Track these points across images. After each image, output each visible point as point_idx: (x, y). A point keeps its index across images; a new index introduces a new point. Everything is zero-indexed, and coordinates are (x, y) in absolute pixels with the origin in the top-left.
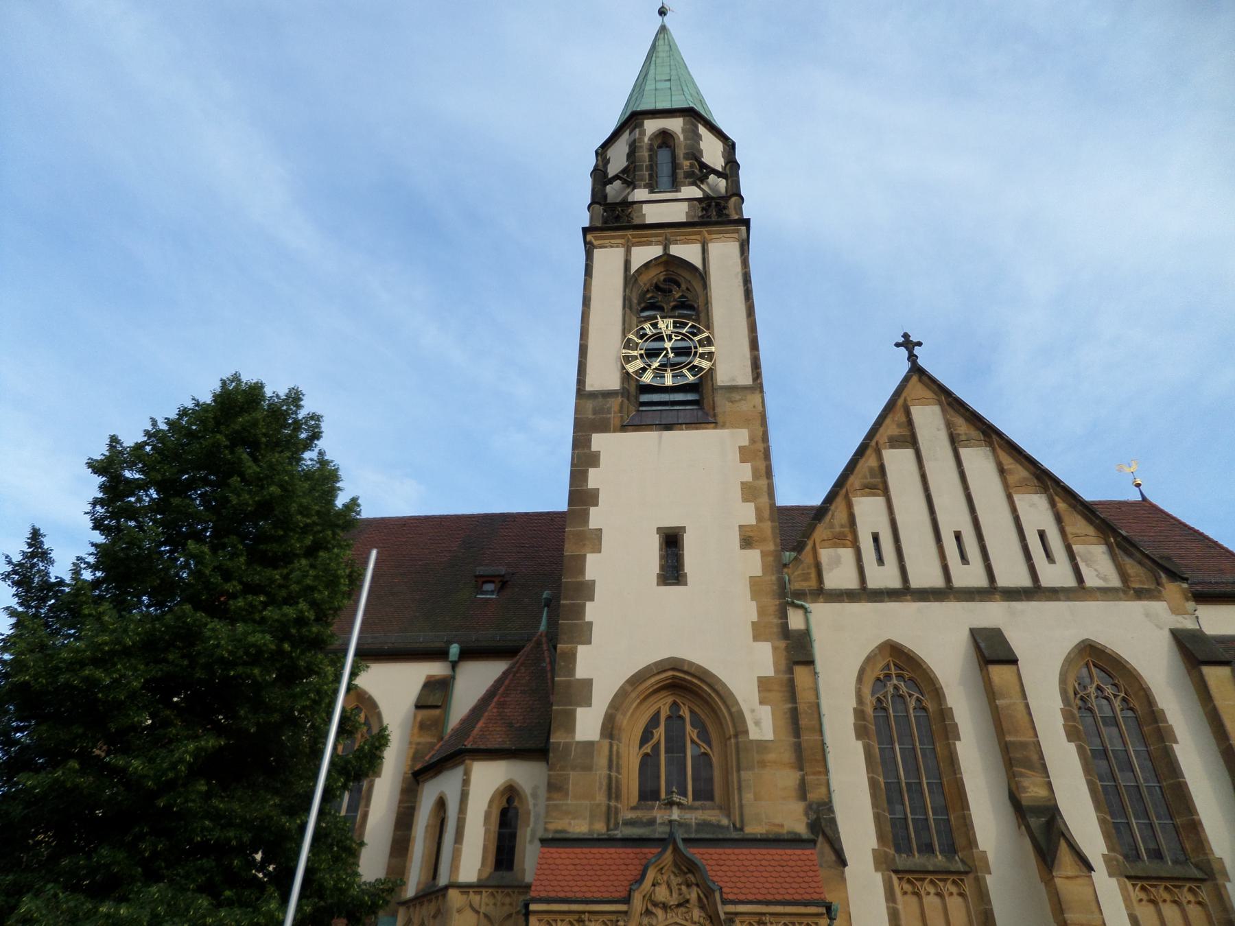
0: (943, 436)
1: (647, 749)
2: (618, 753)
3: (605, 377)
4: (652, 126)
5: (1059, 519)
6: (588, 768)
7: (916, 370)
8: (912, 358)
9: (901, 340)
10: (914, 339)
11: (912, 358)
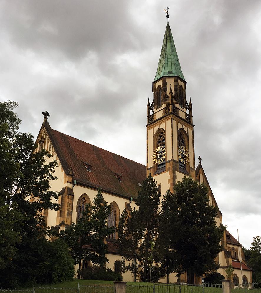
4: (157, 85)
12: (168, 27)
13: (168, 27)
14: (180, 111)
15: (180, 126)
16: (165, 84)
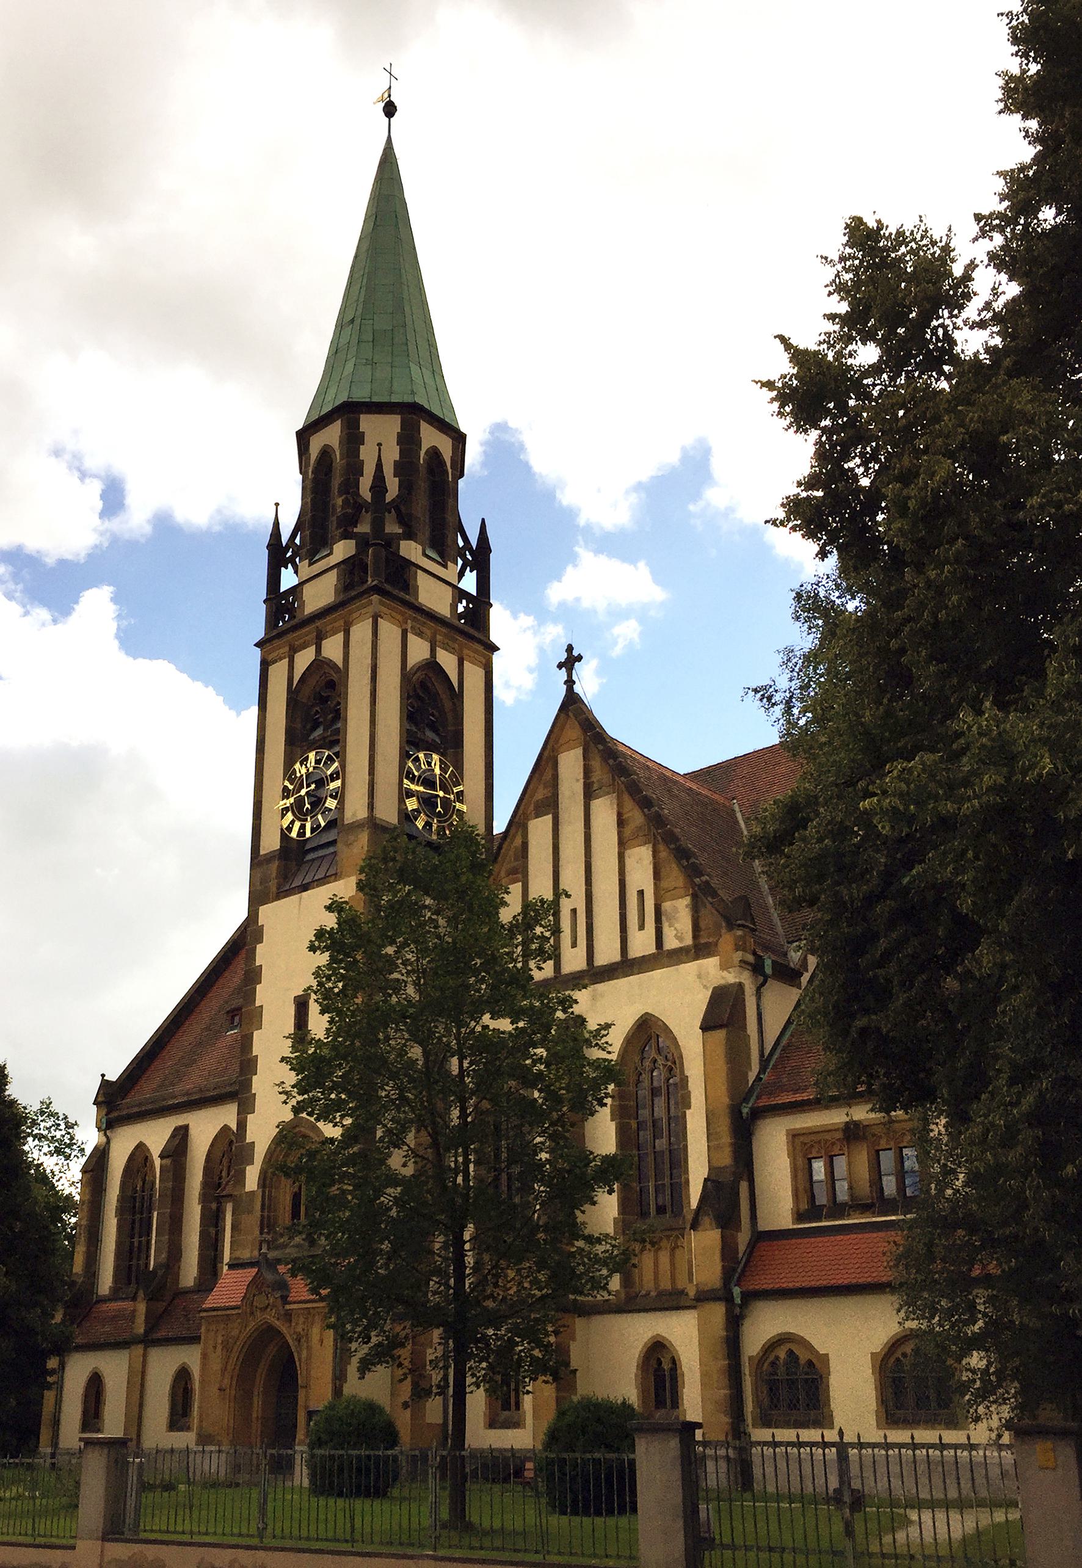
0: (579, 787)
1: (296, 1189)
2: (270, 1196)
3: (271, 843)
5: (657, 875)
6: (250, 1212)
7: (572, 704)
8: (570, 683)
9: (575, 653)
10: (563, 657)
11: (570, 683)
12: (388, 163)
13: (388, 163)
14: (422, 579)
15: (419, 650)
16: (353, 439)
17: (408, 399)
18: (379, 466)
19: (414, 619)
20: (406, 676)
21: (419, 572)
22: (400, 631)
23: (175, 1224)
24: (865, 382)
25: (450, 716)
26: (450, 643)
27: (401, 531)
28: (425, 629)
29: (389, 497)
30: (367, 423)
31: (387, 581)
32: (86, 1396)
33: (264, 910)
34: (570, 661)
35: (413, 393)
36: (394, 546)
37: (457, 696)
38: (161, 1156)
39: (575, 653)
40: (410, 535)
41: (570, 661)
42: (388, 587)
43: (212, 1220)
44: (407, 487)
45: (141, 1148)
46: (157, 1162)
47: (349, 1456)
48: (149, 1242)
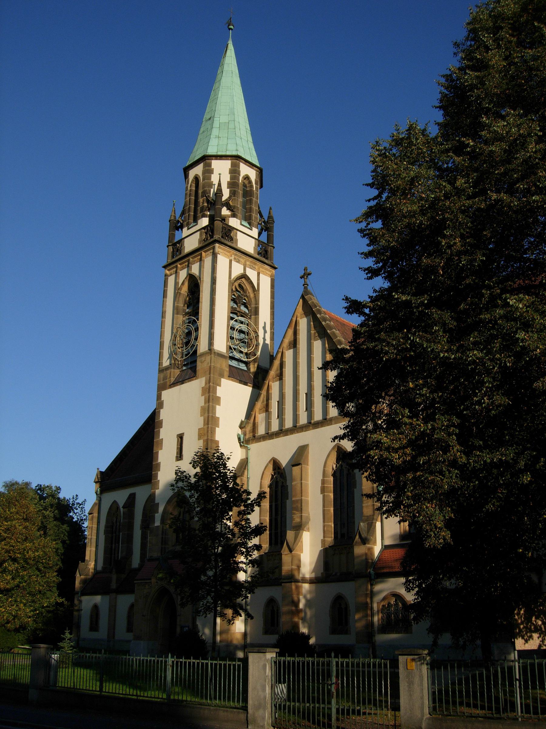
8: (305, 285)
9: (308, 271)
15: (238, 269)
16: (208, 171)
17: (234, 153)
18: (219, 185)
19: (236, 255)
20: (231, 283)
21: (238, 232)
22: (228, 260)
23: (130, 538)
24: (541, 527)
25: (253, 300)
26: (254, 266)
27: (230, 214)
28: (241, 259)
29: (224, 198)
30: (215, 164)
31: (222, 237)
32: (91, 616)
33: (165, 394)
34: (306, 275)
35: (237, 150)
36: (227, 221)
37: (256, 291)
38: (123, 507)
39: (308, 271)
40: (234, 216)
41: (306, 275)
42: (223, 240)
43: (144, 537)
44: (233, 193)
45: (115, 502)
46: (122, 509)
47: (202, 663)
48: (119, 546)
